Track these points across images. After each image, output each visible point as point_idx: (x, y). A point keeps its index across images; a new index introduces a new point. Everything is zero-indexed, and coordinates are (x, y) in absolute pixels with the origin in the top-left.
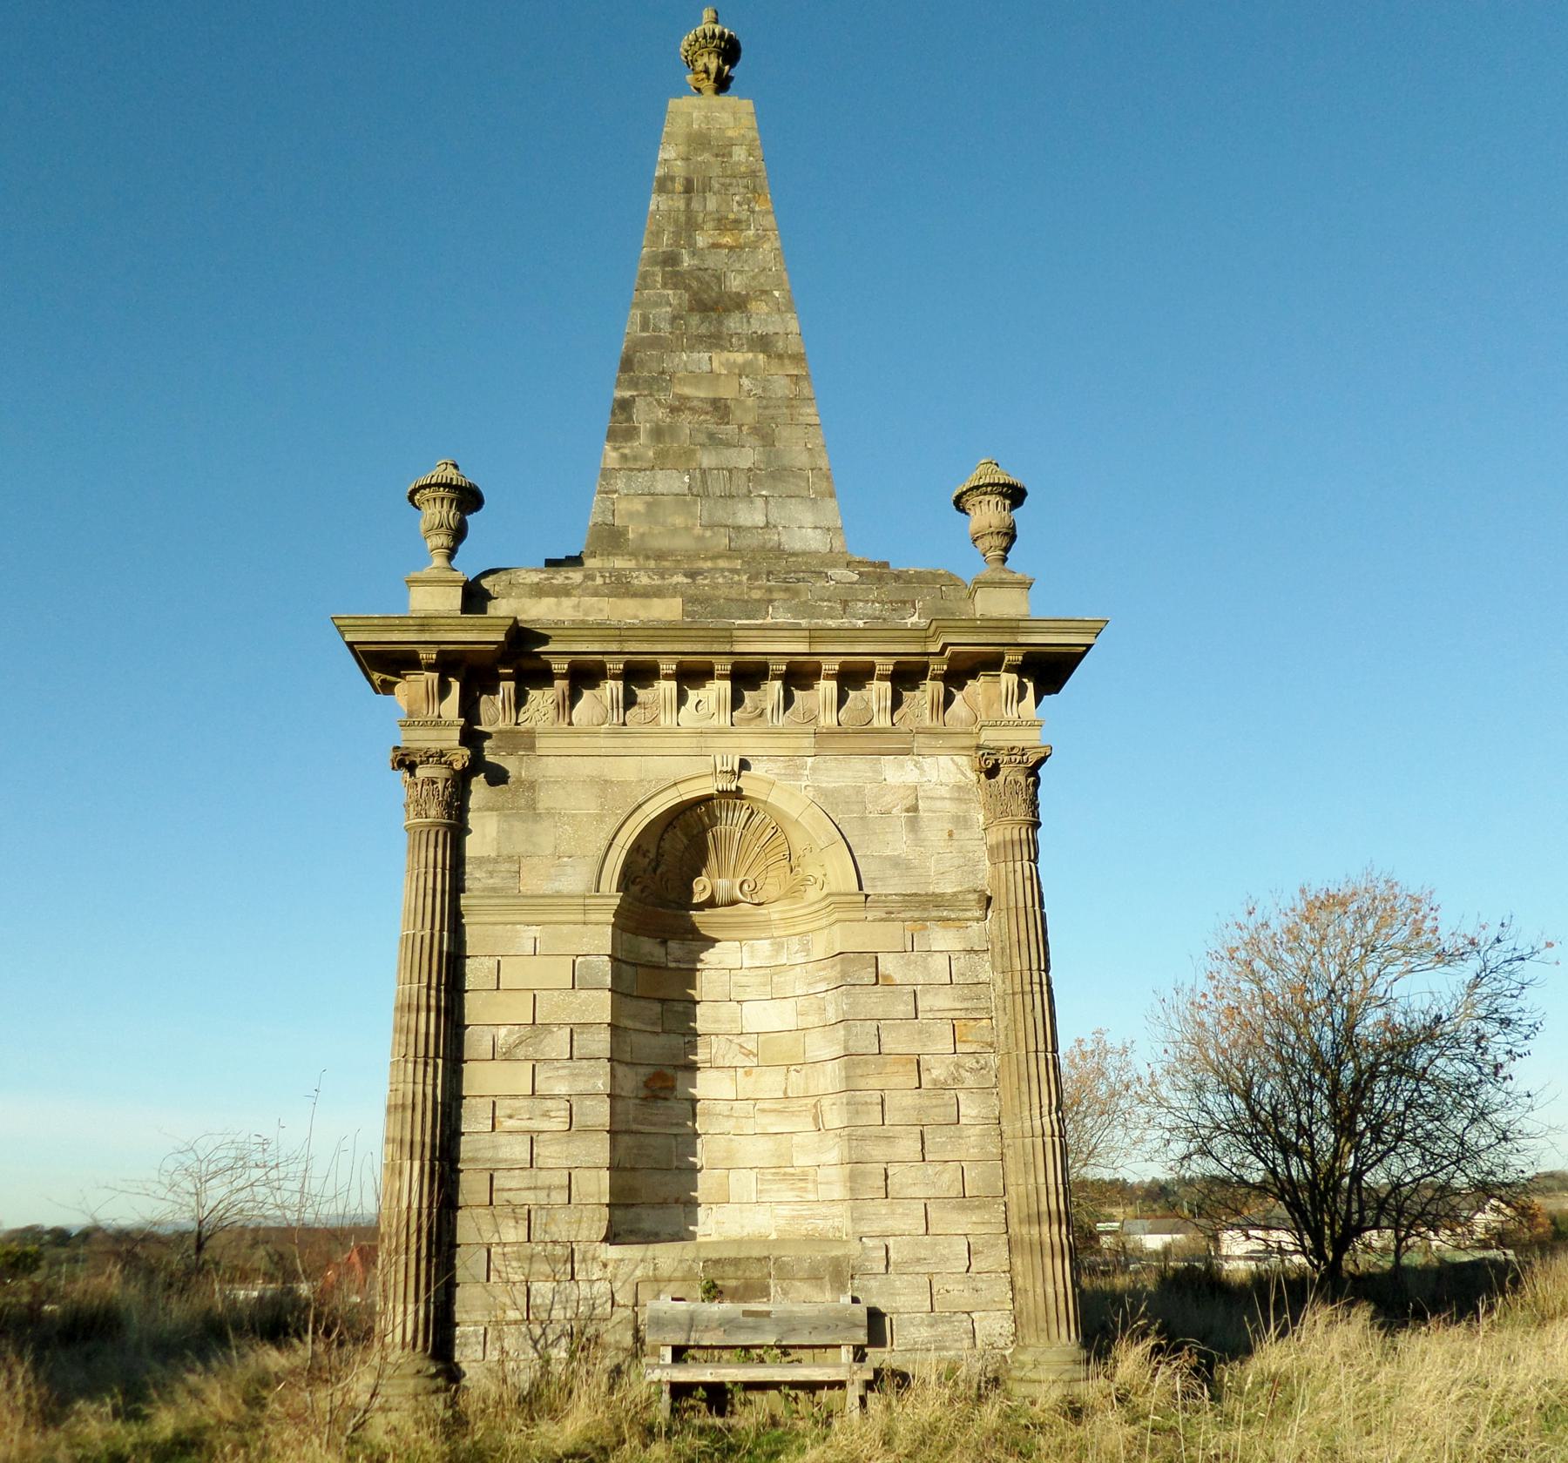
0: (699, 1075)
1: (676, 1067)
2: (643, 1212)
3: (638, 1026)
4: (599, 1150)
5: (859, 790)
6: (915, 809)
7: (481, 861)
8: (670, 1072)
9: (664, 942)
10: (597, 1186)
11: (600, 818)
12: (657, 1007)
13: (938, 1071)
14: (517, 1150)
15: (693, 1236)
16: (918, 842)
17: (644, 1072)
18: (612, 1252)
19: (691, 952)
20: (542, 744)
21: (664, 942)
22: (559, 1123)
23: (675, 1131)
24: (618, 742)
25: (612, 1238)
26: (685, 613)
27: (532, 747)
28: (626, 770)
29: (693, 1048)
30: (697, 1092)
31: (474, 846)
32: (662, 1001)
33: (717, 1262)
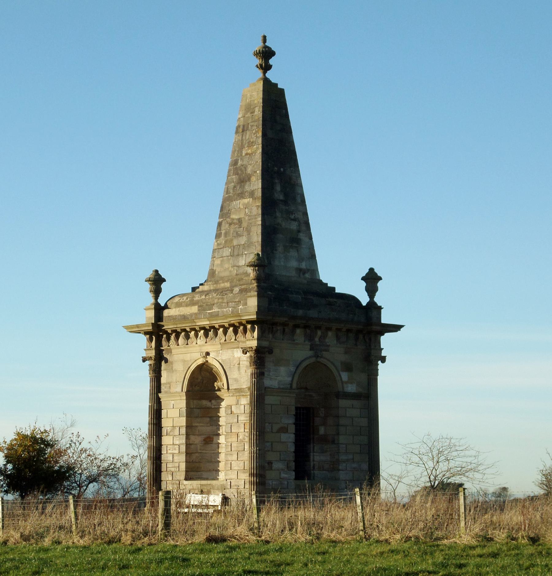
0: (220, 437)
1: (214, 435)
2: (203, 473)
3: (201, 425)
4: (183, 458)
5: (230, 359)
6: (239, 364)
7: (164, 384)
8: (211, 436)
9: (210, 401)
10: (183, 466)
11: (183, 370)
12: (208, 419)
13: (241, 437)
14: (170, 458)
15: (218, 479)
16: (240, 373)
17: (203, 437)
18: (186, 482)
19: (218, 403)
20: (173, 351)
21: (210, 401)
22: (177, 452)
23: (213, 452)
24: (186, 350)
25: (186, 479)
26: (199, 310)
27: (171, 352)
28: (188, 357)
29: (219, 429)
30: (220, 441)
31: (163, 380)
32: (210, 417)
33: (417, 491)
